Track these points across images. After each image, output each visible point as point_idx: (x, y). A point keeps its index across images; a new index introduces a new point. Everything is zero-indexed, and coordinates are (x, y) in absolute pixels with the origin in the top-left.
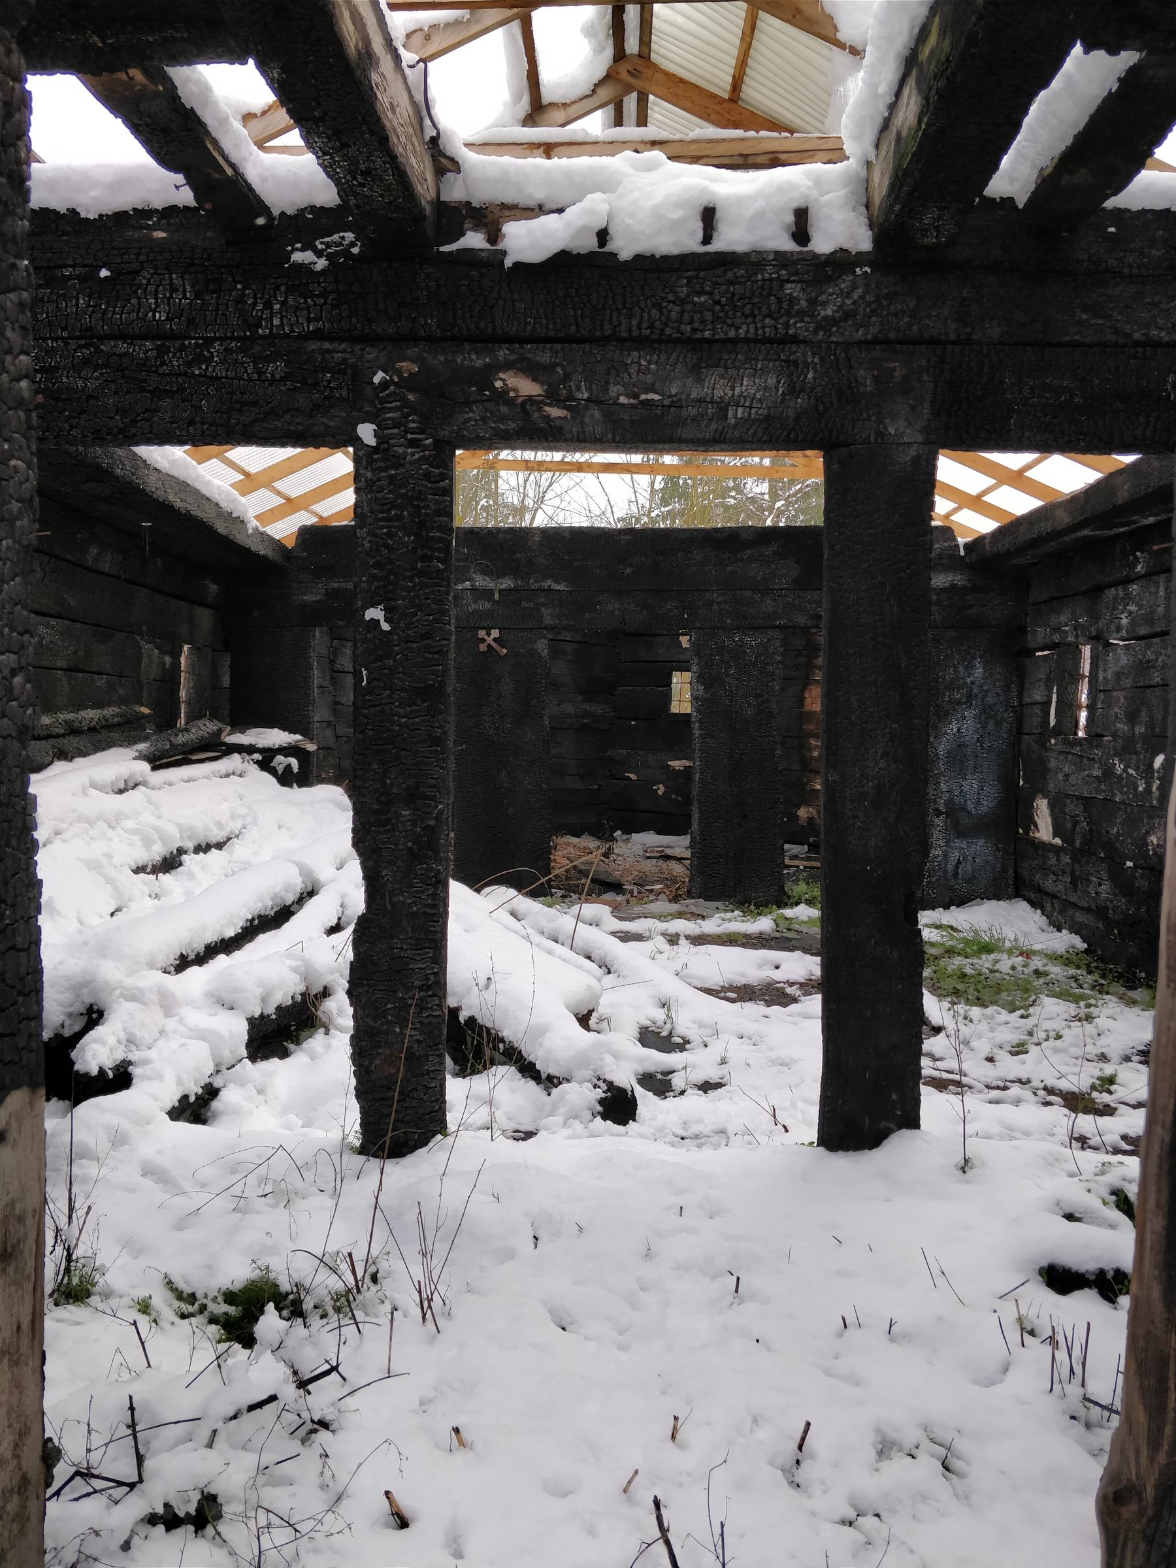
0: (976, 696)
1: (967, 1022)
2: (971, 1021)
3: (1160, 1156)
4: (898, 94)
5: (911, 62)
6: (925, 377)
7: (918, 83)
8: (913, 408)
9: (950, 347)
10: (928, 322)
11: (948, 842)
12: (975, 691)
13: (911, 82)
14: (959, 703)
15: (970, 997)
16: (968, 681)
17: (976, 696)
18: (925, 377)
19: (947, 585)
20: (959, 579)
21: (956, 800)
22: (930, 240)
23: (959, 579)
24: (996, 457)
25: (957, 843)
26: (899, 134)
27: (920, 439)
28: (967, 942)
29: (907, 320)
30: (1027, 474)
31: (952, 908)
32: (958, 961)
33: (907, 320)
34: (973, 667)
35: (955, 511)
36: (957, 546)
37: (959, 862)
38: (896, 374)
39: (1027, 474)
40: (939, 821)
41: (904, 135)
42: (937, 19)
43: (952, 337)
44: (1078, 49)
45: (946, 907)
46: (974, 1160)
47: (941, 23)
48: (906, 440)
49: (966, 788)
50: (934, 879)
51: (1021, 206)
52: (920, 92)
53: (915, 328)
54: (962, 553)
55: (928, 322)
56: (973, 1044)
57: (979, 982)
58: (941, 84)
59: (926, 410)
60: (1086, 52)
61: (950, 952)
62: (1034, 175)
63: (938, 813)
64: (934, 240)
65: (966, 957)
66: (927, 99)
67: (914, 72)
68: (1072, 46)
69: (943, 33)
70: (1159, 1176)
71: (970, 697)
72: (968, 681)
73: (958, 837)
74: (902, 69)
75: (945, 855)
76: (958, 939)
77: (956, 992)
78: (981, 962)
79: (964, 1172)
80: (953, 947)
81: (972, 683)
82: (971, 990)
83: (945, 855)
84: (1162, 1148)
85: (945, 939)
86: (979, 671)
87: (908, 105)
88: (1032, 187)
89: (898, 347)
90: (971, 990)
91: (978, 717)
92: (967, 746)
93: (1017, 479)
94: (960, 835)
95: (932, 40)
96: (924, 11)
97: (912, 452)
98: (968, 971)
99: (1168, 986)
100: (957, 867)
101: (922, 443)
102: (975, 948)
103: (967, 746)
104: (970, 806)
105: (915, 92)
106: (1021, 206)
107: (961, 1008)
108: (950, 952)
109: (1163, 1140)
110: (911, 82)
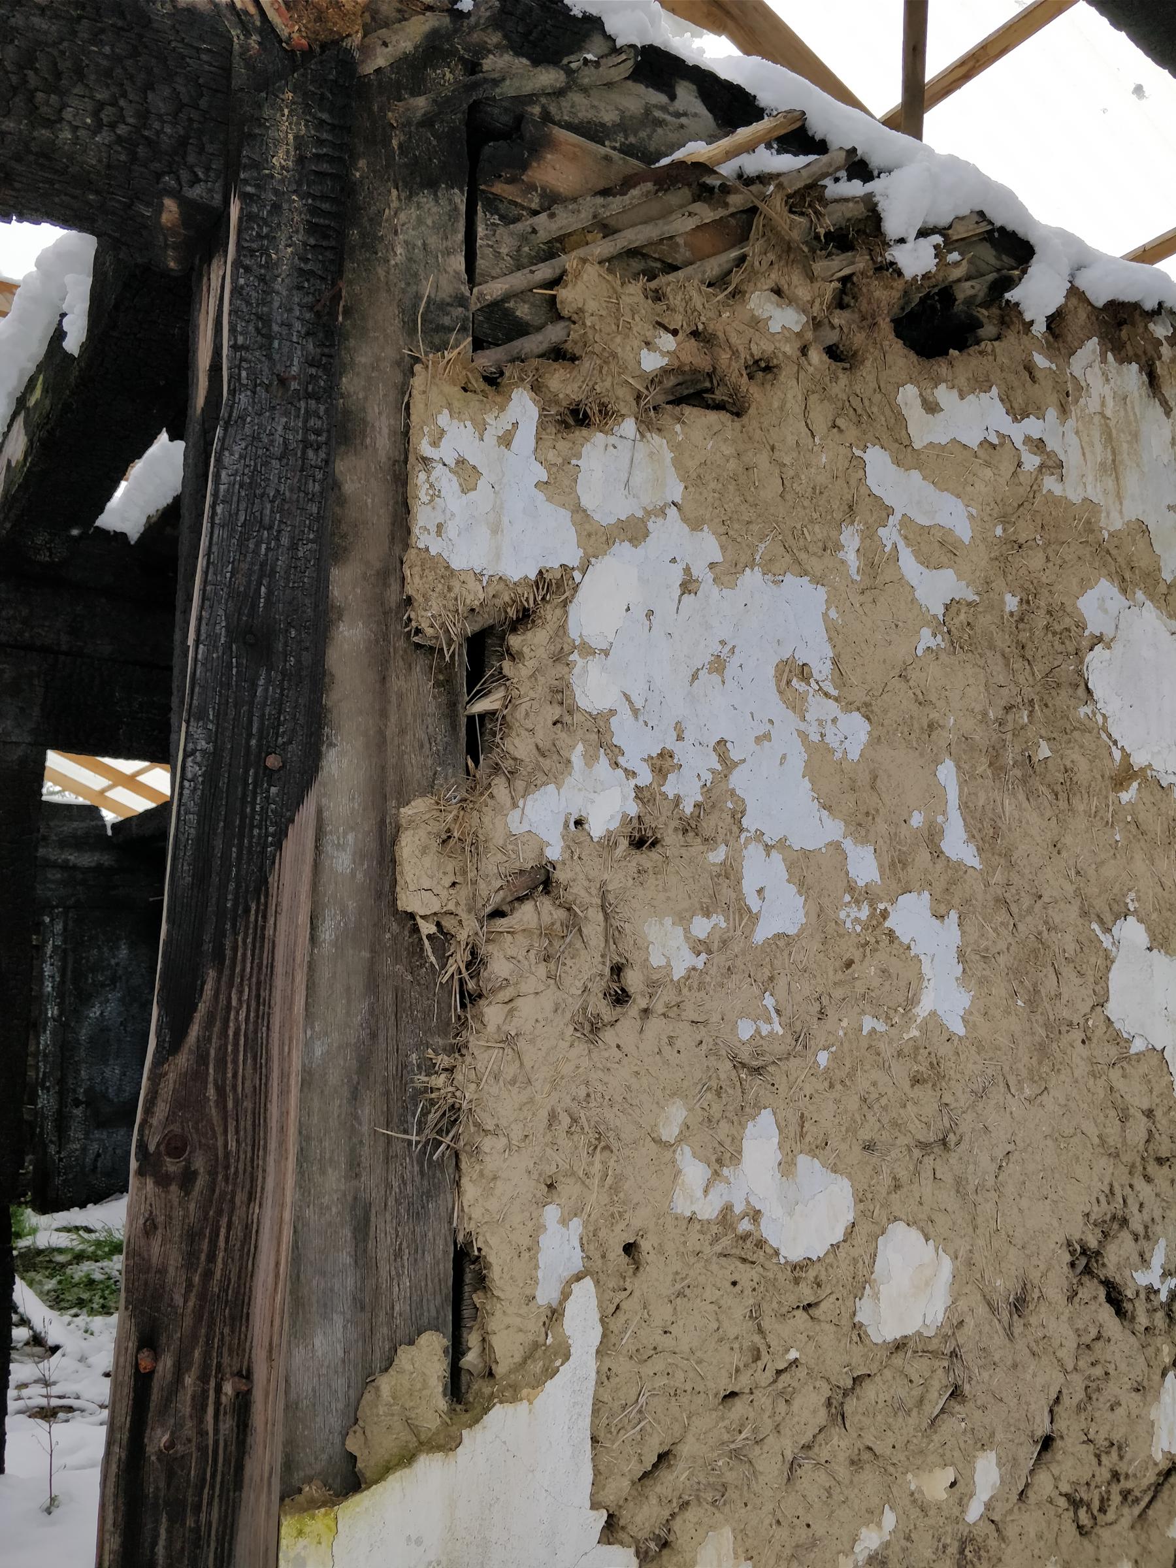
0: (120, 978)
1: (87, 1335)
2: (92, 1334)
3: (117, 1475)
4: (10, 426)
5: (21, 402)
6: (36, 682)
7: (26, 424)
8: (22, 709)
9: (62, 658)
10: (40, 630)
11: (87, 1134)
12: (120, 972)
13: (20, 421)
14: (103, 985)
15: (95, 1306)
16: (113, 962)
17: (120, 978)
18: (36, 682)
19: (93, 864)
20: (106, 859)
21: (98, 1088)
22: (44, 557)
23: (106, 859)
24: (107, 761)
25: (97, 1134)
26: (9, 461)
27: (28, 739)
28: (98, 1244)
29: (18, 626)
30: (138, 778)
31: (90, 1206)
32: (87, 1267)
33: (18, 626)
34: (118, 948)
35: (110, 788)
36: (105, 826)
37: (98, 1155)
38: (6, 676)
39: (138, 778)
40: (78, 1112)
41: (13, 464)
42: (41, 377)
43: (64, 647)
44: (164, 437)
45: (82, 1206)
46: (60, 1498)
47: (44, 382)
48: (14, 739)
49: (108, 1073)
50: (71, 1176)
51: (132, 543)
52: (26, 434)
53: (27, 634)
54: (109, 833)
55: (40, 630)
56: (91, 1360)
57: (108, 1287)
58: (43, 434)
59: (36, 712)
60: (171, 439)
61: (79, 1257)
62: (143, 520)
63: (77, 1103)
64: (47, 559)
65: (97, 1261)
66: (31, 441)
67: (23, 414)
68: (159, 432)
69: (45, 391)
70: (116, 1496)
71: (114, 980)
72: (113, 962)
73: (98, 1127)
74: (13, 407)
75: (84, 1149)
76: (89, 1241)
77: (81, 1303)
78: (111, 1264)
79: (50, 1513)
80: (83, 1251)
81: (117, 964)
82: (97, 1299)
83: (84, 1149)
84: (119, 1466)
85: (75, 1243)
86: (124, 952)
87: (17, 440)
88: (142, 529)
89: (8, 650)
90: (97, 1299)
91: (122, 1000)
92: (110, 1030)
93: (131, 782)
94: (100, 1125)
95: (38, 393)
96: (31, 368)
97: (20, 752)
98: (98, 1276)
99: (126, 1308)
100: (96, 1160)
101: (30, 744)
102: (107, 1249)
103: (110, 1030)
104: (111, 1092)
105: (23, 431)
106: (132, 543)
107: (83, 1320)
108: (79, 1257)
109: (120, 1459)
110: (20, 421)
